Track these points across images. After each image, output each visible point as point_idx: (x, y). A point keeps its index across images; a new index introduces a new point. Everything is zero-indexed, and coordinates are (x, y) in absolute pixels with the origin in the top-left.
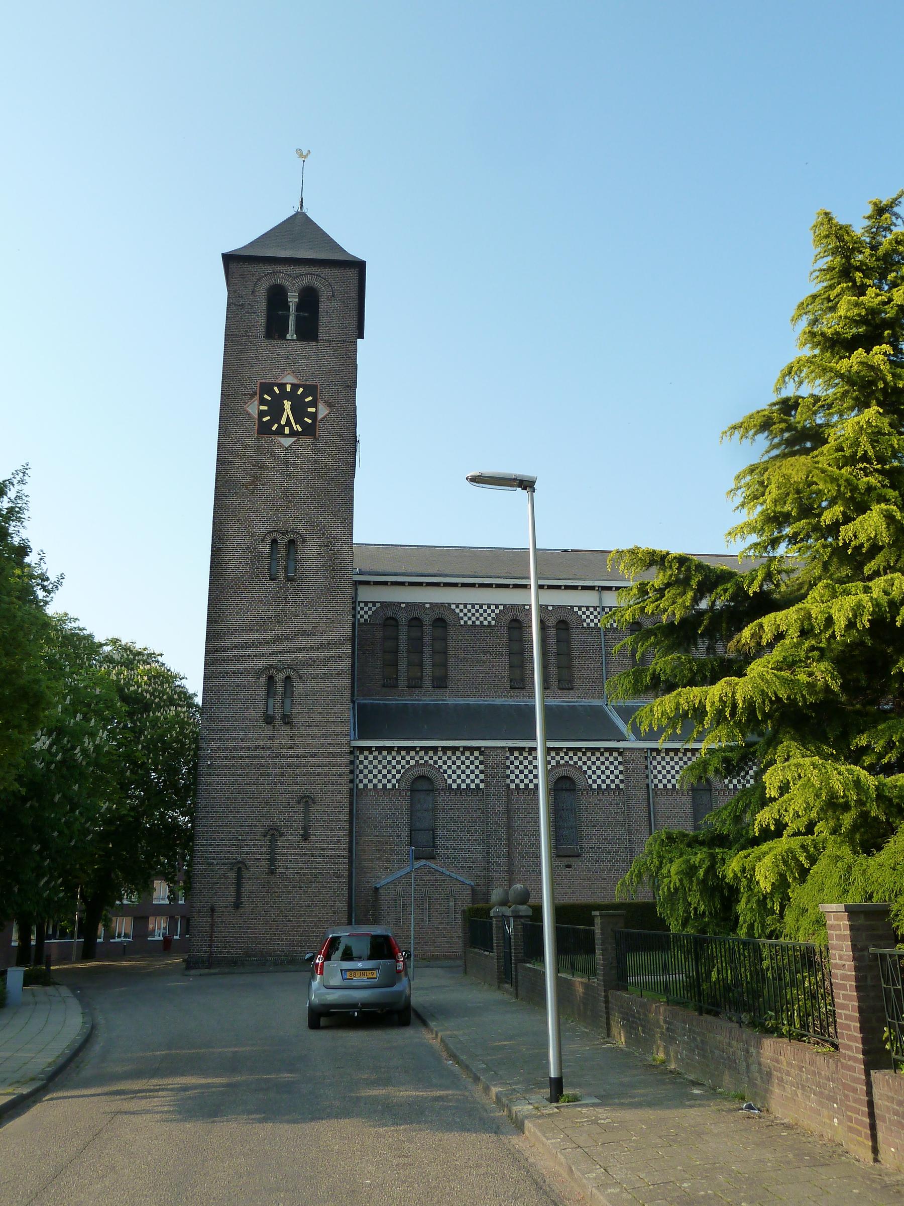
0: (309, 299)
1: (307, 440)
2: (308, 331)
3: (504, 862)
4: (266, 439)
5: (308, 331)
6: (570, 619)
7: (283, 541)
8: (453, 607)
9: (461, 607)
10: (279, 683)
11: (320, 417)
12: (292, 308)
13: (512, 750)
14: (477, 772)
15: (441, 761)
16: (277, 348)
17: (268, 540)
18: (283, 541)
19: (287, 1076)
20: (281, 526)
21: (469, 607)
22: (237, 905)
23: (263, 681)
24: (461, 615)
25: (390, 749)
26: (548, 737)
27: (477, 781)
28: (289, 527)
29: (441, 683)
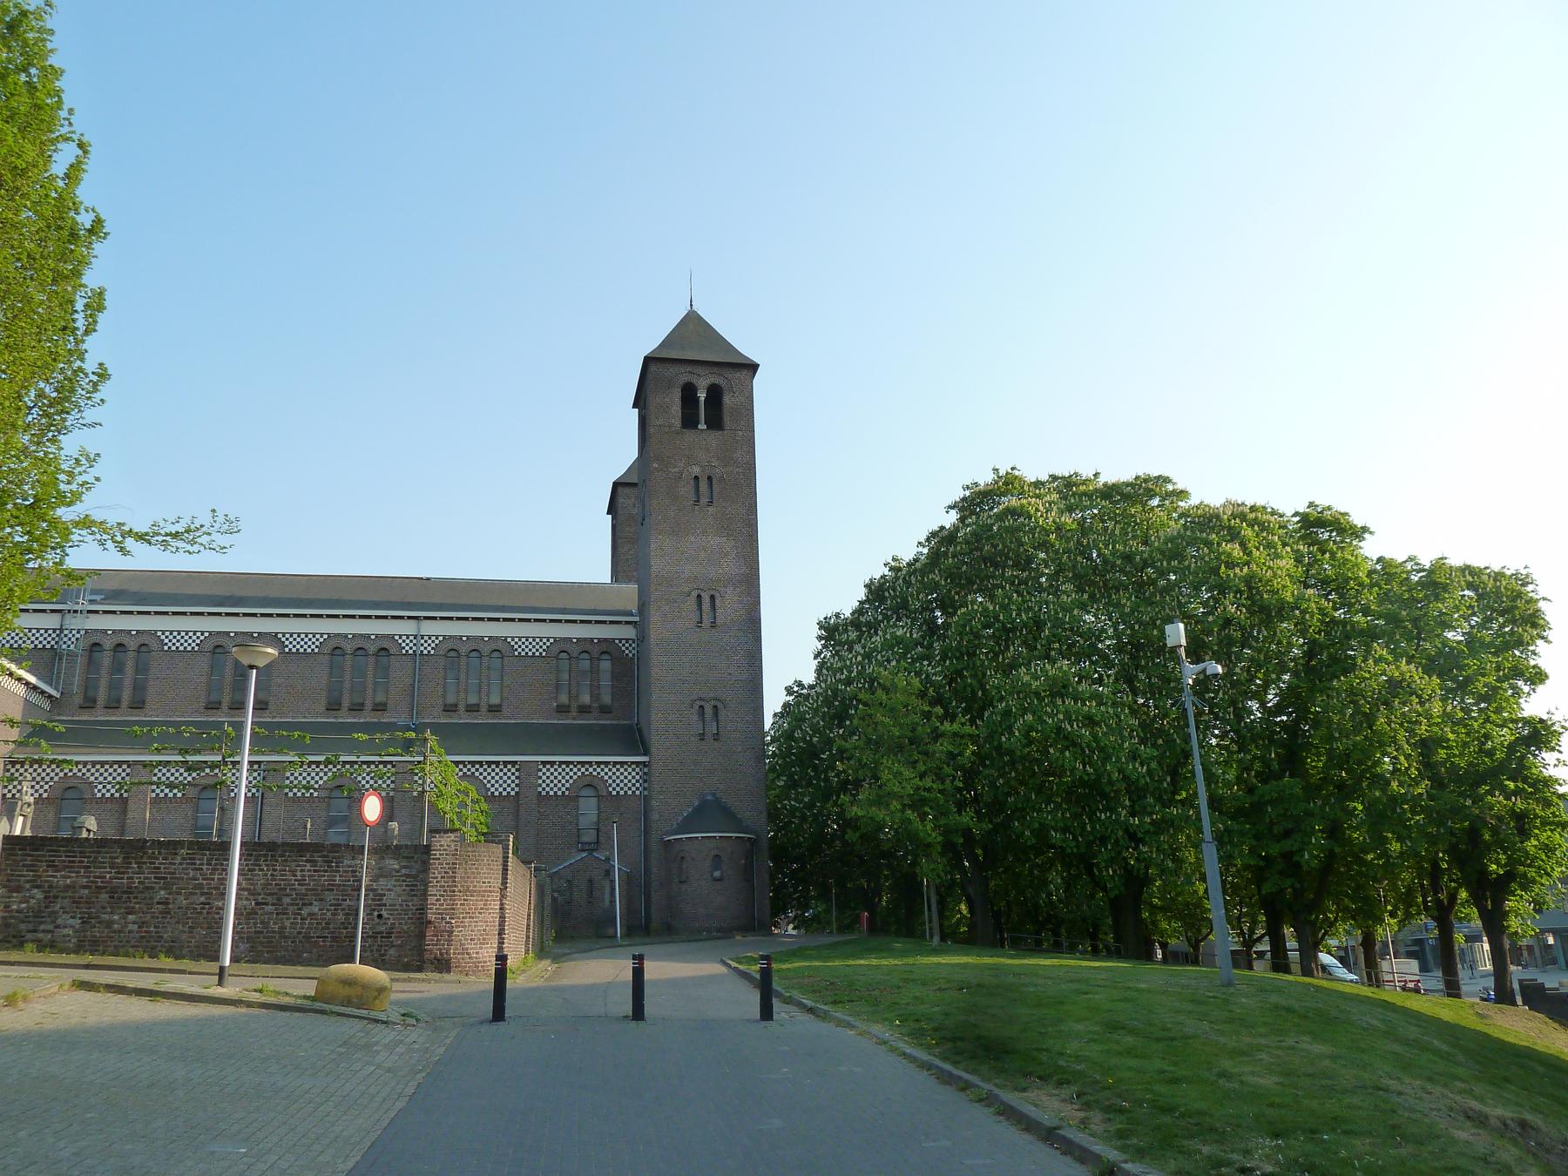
0: (715, 393)
2: (715, 422)
5: (715, 422)
10: (709, 710)
13: (544, 763)
15: (604, 772)
16: (689, 435)
19: (1294, 956)
25: (552, 763)
26: (252, 752)
29: (138, 704)
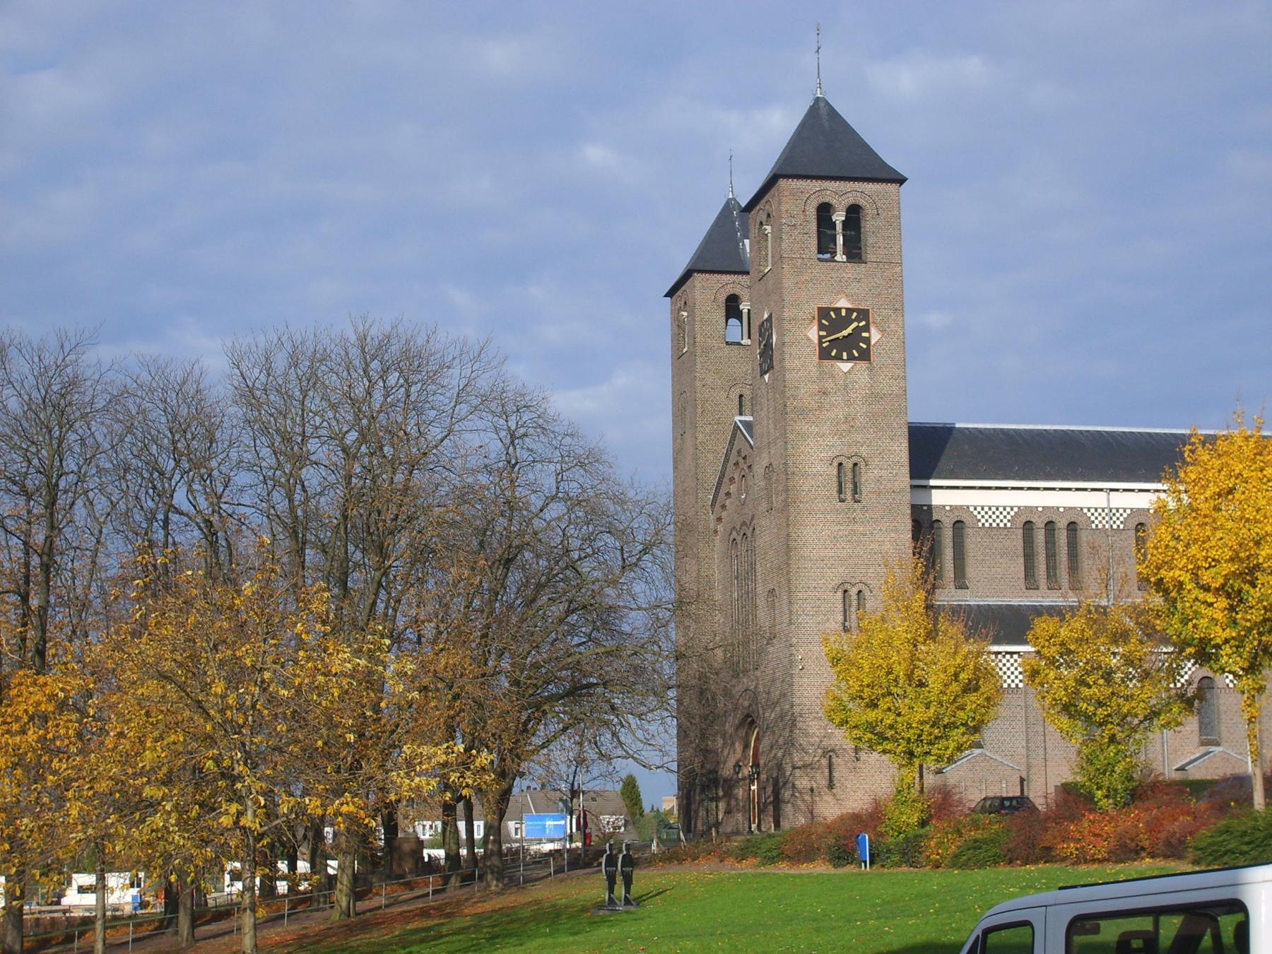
1: (863, 365)
2: (855, 252)
3: (1041, 752)
4: (826, 362)
6: (1080, 520)
7: (848, 465)
8: (972, 509)
9: (979, 509)
11: (873, 342)
12: (839, 227)
14: (1016, 673)
17: (835, 464)
18: (848, 465)
20: (845, 451)
21: (986, 509)
22: (831, 786)
23: (840, 594)
24: (979, 517)
27: (1017, 681)
28: (854, 450)
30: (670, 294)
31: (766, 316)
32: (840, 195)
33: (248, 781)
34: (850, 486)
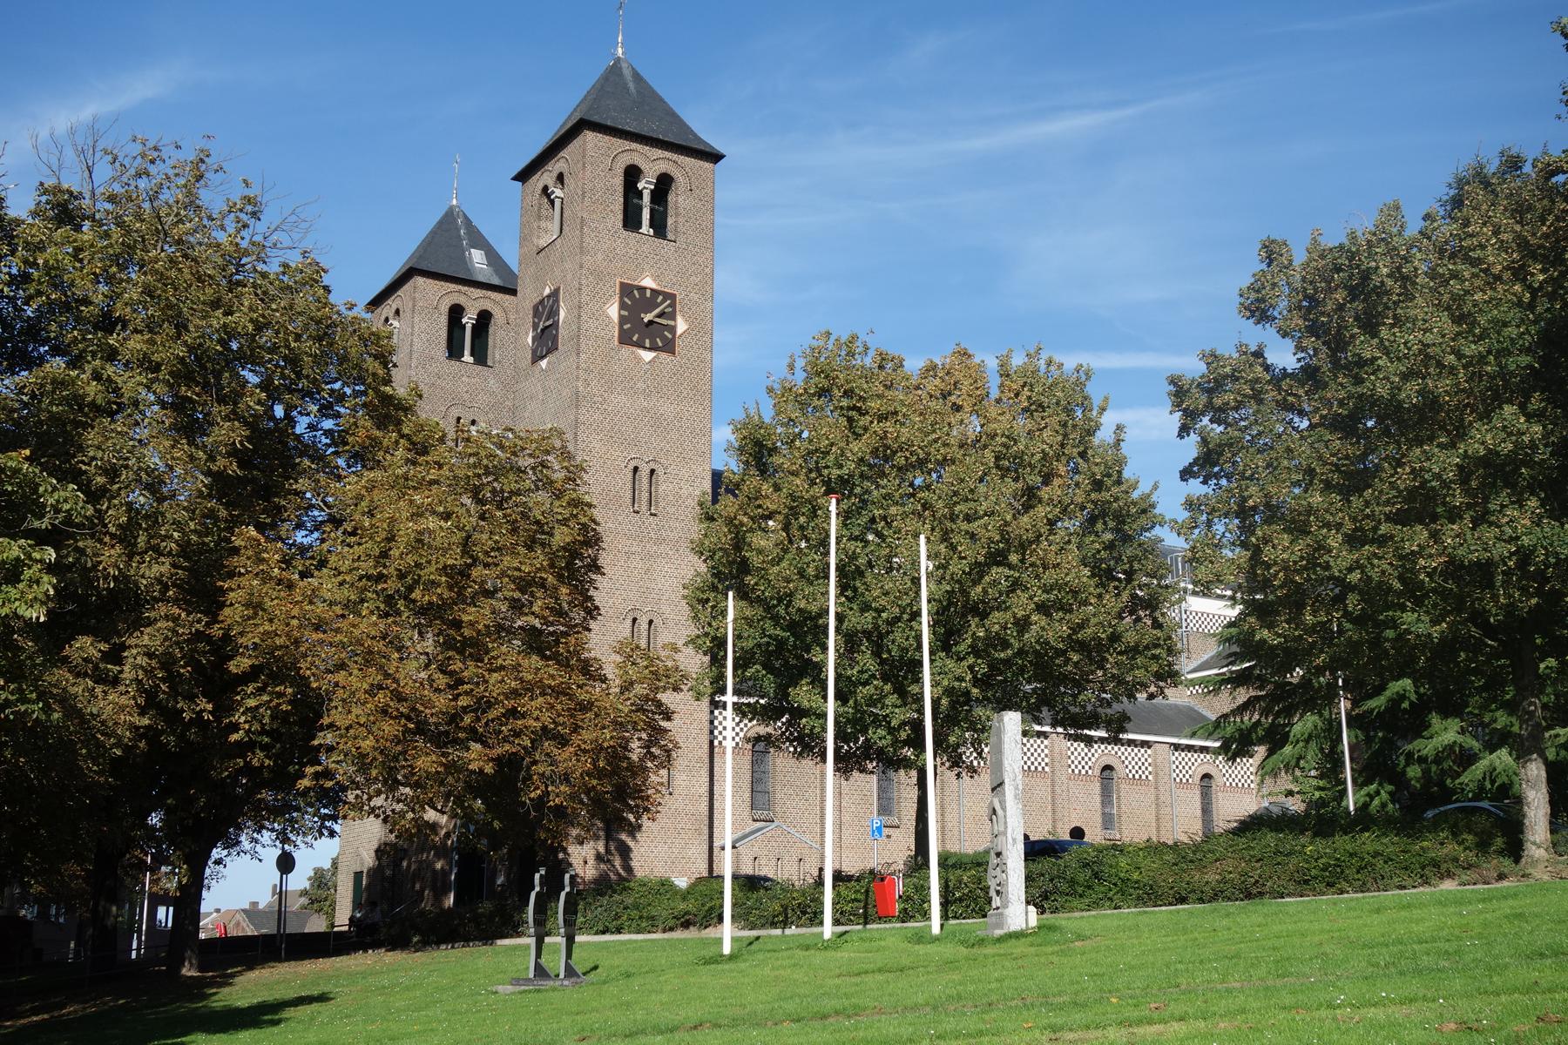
2: (481, 356)
17: (631, 467)
23: (629, 622)
30: (523, 176)
31: (547, 291)
32: (653, 162)
33: (775, 497)
34: (645, 495)
